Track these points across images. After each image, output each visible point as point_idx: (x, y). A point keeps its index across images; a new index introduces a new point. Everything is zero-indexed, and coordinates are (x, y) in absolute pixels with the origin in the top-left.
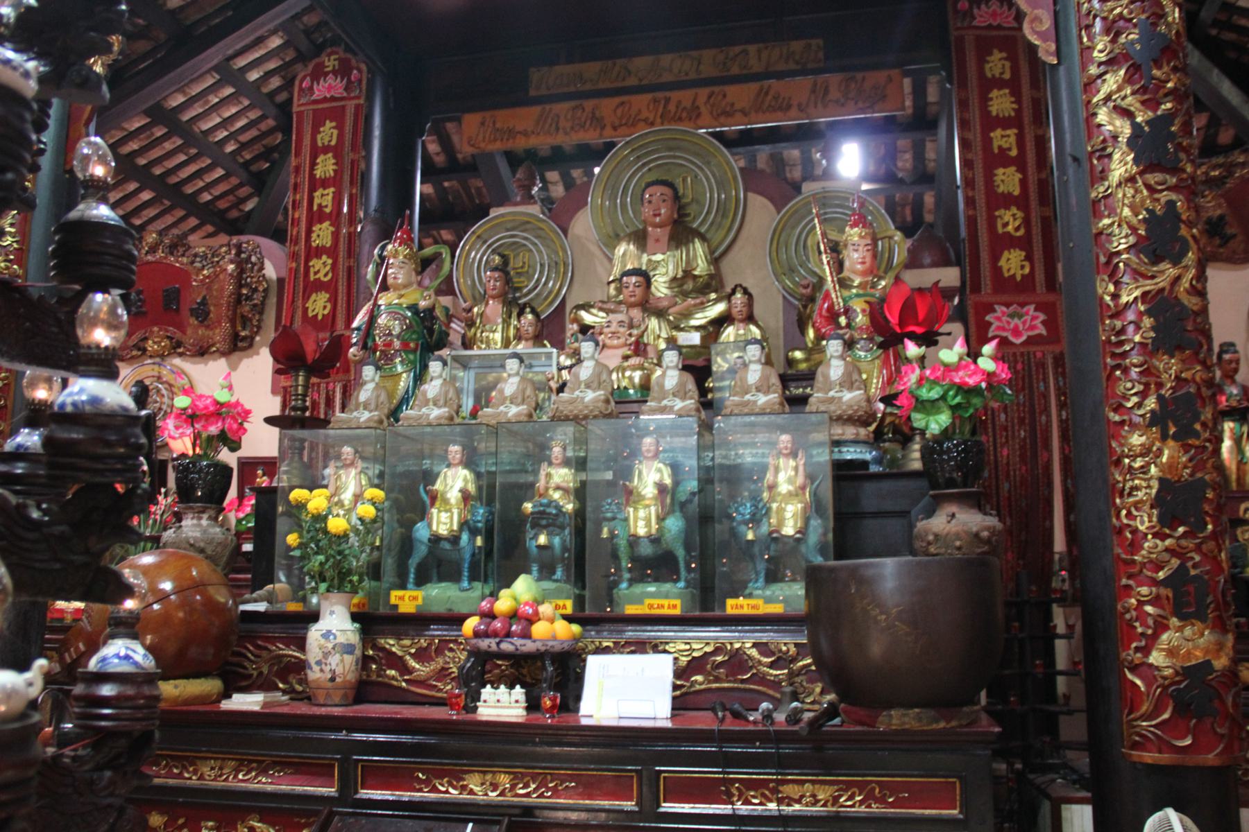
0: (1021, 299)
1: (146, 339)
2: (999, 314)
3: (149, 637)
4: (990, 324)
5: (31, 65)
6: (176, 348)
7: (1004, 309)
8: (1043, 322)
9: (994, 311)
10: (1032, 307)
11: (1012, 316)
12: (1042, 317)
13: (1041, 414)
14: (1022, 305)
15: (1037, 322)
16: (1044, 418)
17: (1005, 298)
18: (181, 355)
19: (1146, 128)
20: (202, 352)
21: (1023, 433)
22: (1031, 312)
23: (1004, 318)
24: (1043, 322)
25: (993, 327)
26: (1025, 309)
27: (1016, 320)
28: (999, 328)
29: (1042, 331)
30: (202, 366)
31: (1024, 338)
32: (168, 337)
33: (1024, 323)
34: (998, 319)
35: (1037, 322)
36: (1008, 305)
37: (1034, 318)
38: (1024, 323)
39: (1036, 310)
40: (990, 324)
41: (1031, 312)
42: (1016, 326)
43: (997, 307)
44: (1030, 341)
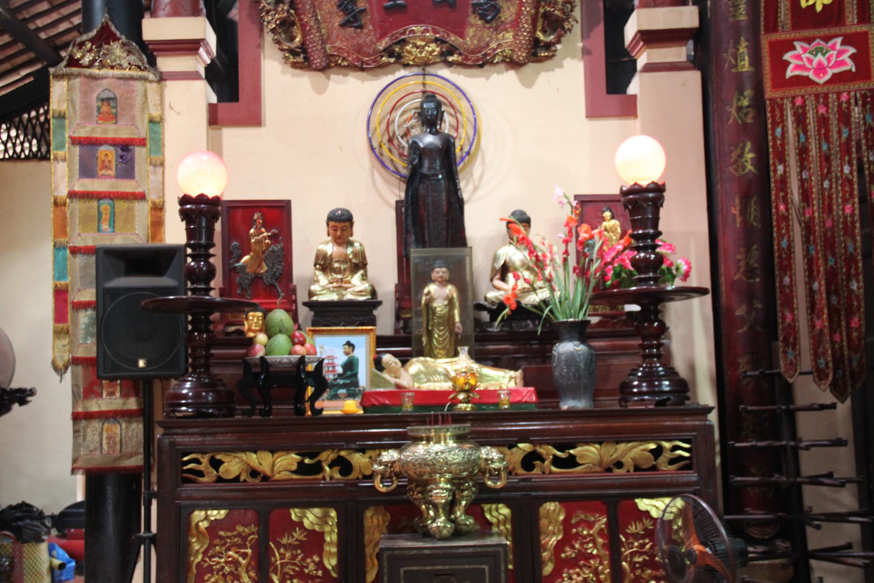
0: (824, 32)
1: (404, 42)
2: (799, 51)
3: (471, 521)
4: (787, 63)
5: (749, 167)
6: (447, 54)
7: (806, 45)
8: (852, 57)
9: (794, 48)
10: (839, 40)
11: (815, 52)
12: (852, 50)
13: (775, 125)
14: (827, 39)
15: (845, 57)
16: (779, 130)
17: (807, 33)
18: (450, 64)
19: (334, 575)
20: (480, 61)
21: (846, 169)
22: (838, 47)
23: (804, 56)
24: (852, 57)
25: (791, 67)
26: (830, 44)
27: (819, 56)
28: (797, 67)
29: (850, 66)
30: (483, 80)
31: (828, 77)
32: (436, 40)
33: (829, 60)
34: (798, 57)
35: (845, 57)
36: (809, 40)
37: (841, 53)
38: (829, 60)
39: (843, 43)
40: (787, 63)
41: (838, 47)
42: (820, 64)
43: (795, 43)
44: (837, 78)
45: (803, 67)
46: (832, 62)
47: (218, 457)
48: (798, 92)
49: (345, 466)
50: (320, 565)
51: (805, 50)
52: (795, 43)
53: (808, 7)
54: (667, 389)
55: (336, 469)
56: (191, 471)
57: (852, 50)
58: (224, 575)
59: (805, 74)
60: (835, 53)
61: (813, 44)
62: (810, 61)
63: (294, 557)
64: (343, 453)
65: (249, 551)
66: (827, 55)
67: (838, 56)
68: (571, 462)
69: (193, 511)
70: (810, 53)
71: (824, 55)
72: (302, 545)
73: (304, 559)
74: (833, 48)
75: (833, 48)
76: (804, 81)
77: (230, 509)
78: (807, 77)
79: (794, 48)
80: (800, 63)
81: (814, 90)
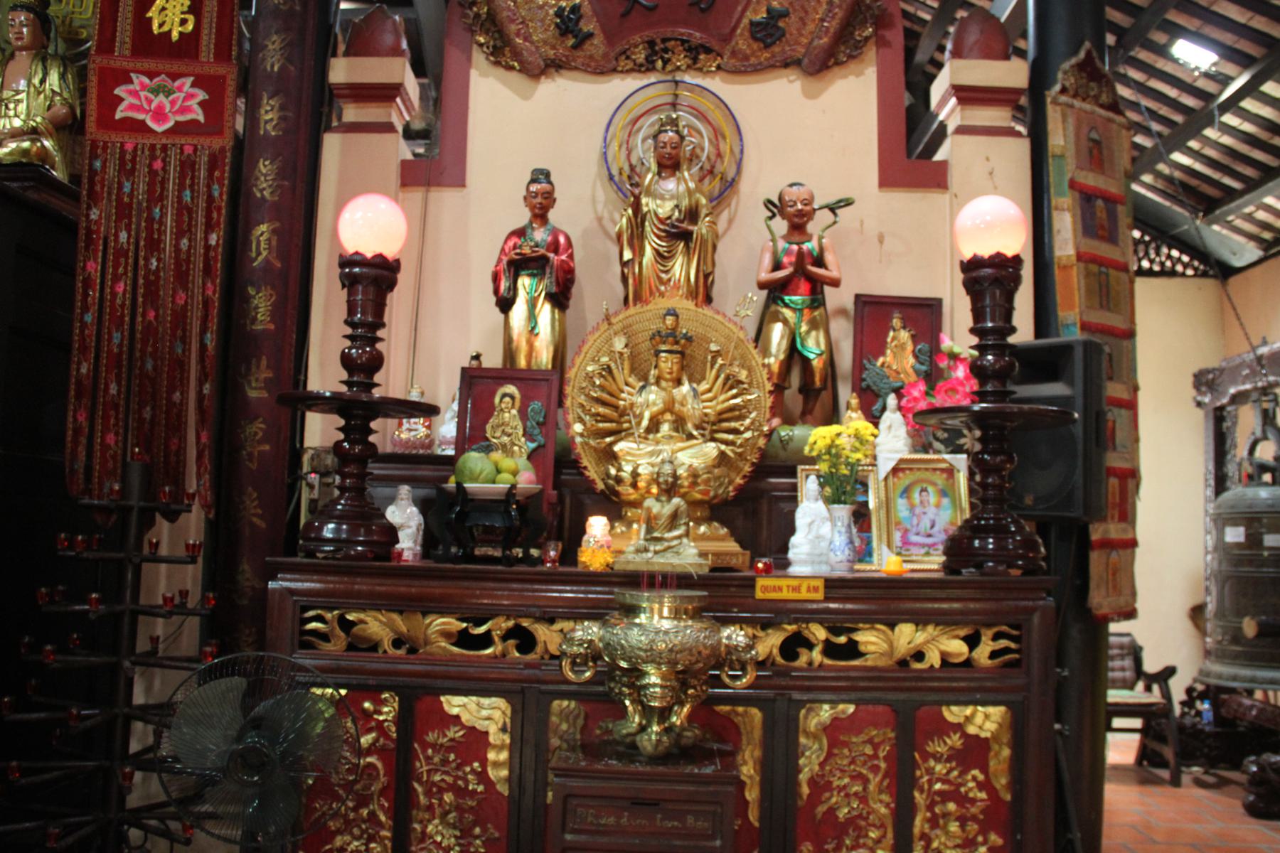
8: (201, 104)
10: (190, 80)
11: (156, 92)
12: (202, 95)
14: (174, 77)
15: (193, 103)
22: (187, 88)
23: (142, 94)
24: (201, 104)
26: (177, 83)
27: (161, 97)
28: (132, 107)
31: (170, 124)
33: (173, 103)
34: (135, 94)
35: (193, 103)
36: (151, 75)
37: (190, 96)
39: (193, 85)
41: (187, 88)
43: (132, 75)
44: (179, 129)
45: (184, 110)
46: (177, 107)
47: (350, 617)
48: (190, 140)
49: (526, 641)
50: (482, 777)
51: (143, 87)
52: (132, 75)
53: (160, 34)
54: (330, 535)
55: (512, 642)
56: (314, 632)
57: (202, 95)
58: (847, 795)
59: (140, 116)
60: (182, 95)
61: (156, 80)
62: (150, 102)
63: (445, 762)
64: (525, 623)
65: (883, 765)
66: (171, 98)
67: (185, 99)
68: (852, 650)
69: (551, 702)
70: (151, 91)
71: (167, 96)
72: (454, 746)
73: (459, 767)
74: (180, 89)
75: (180, 89)
76: (141, 127)
77: (857, 705)
78: (143, 122)
79: (131, 82)
80: (136, 102)
81: (149, 141)
